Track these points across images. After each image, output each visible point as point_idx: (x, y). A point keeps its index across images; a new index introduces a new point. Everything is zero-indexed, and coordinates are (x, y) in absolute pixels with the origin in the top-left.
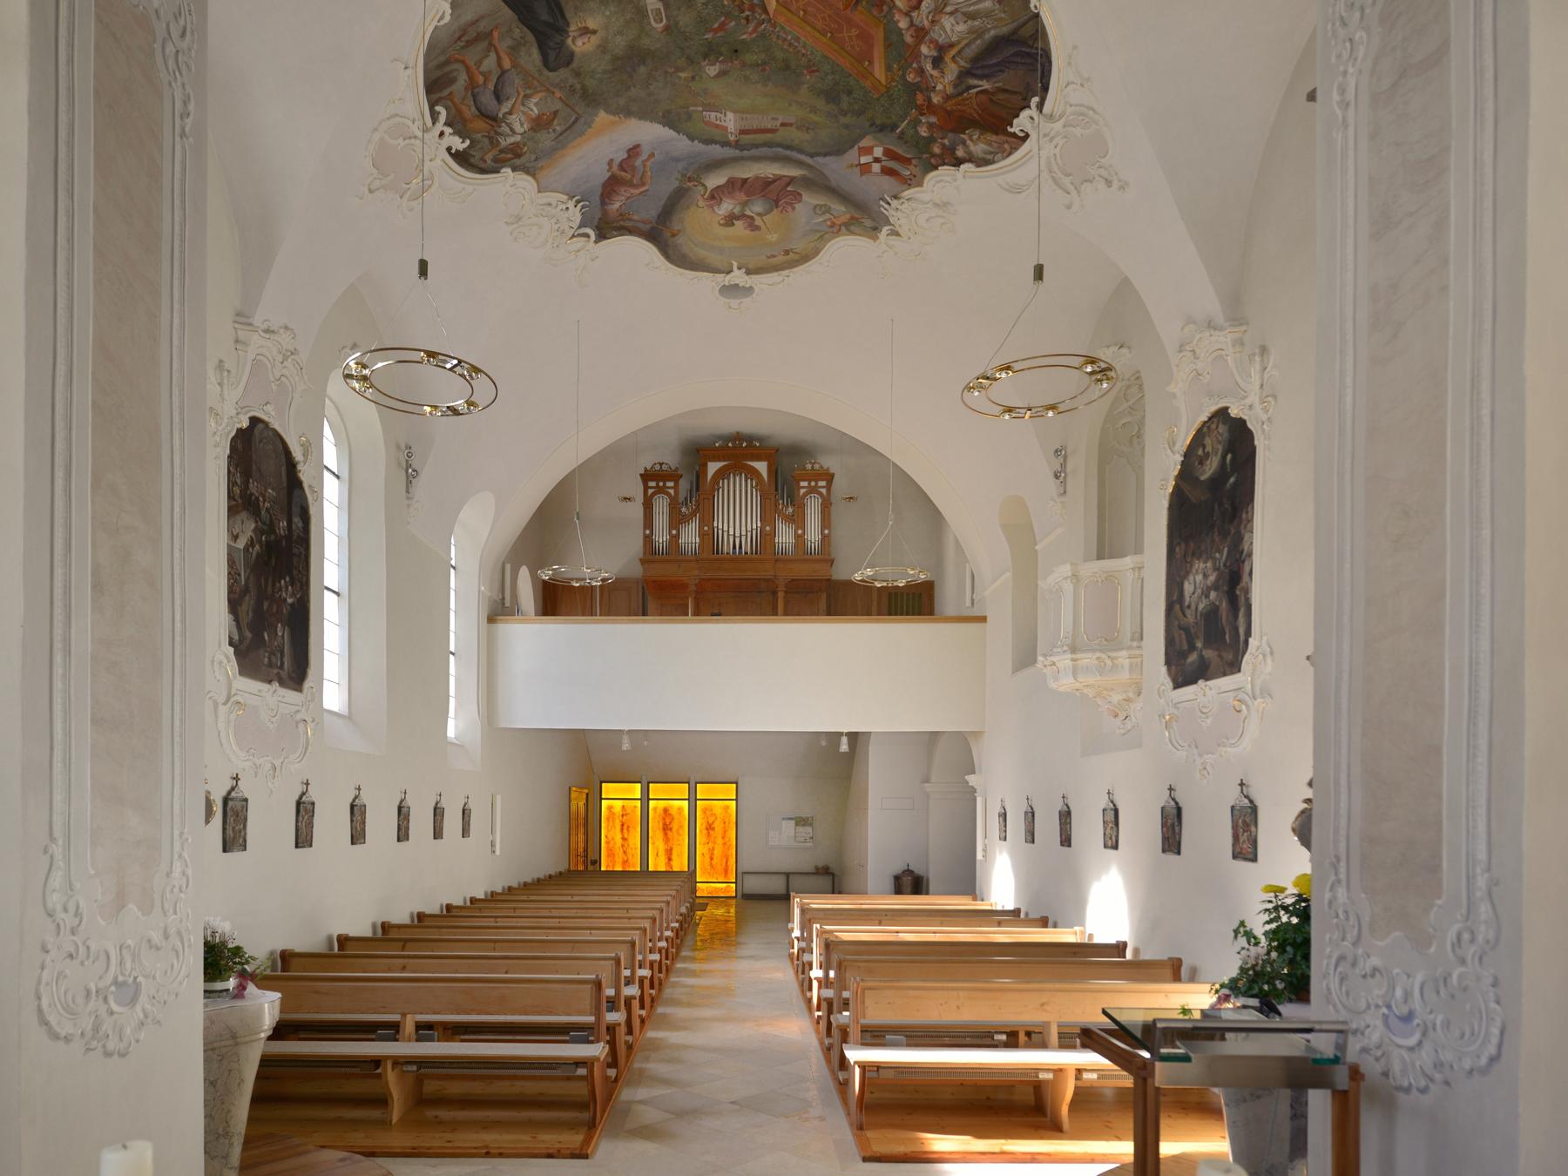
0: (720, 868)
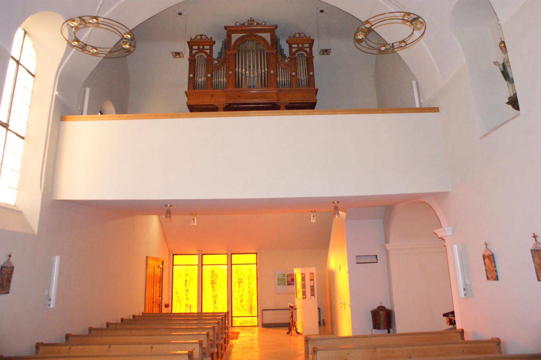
0: (247, 308)
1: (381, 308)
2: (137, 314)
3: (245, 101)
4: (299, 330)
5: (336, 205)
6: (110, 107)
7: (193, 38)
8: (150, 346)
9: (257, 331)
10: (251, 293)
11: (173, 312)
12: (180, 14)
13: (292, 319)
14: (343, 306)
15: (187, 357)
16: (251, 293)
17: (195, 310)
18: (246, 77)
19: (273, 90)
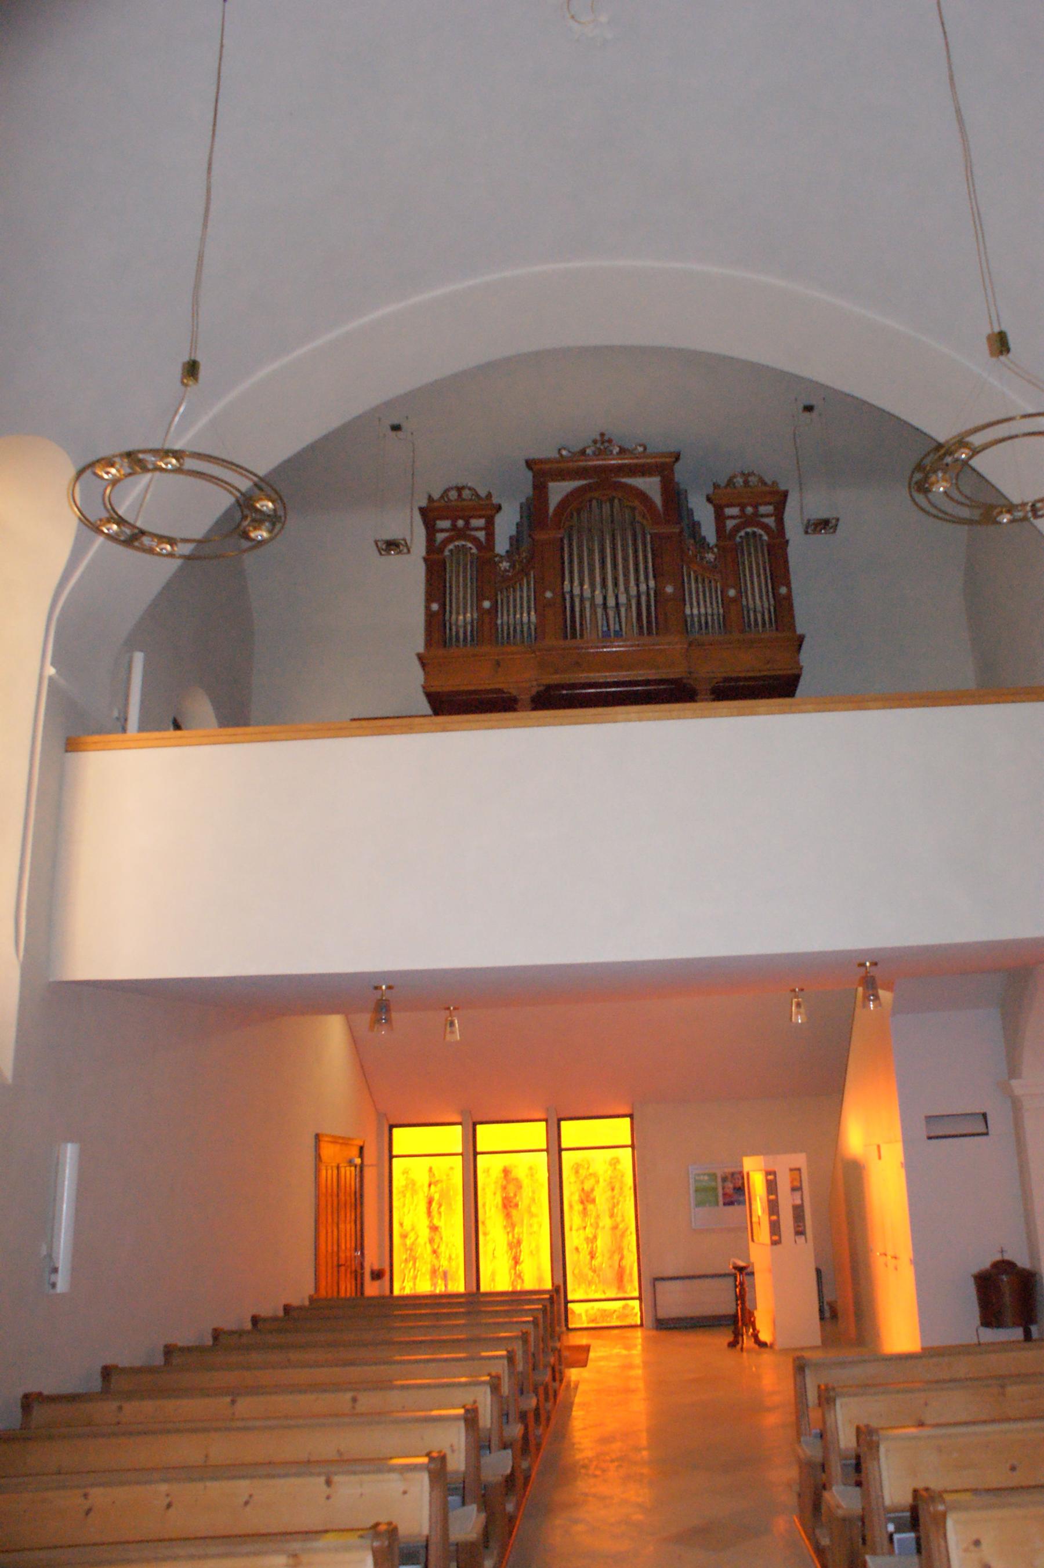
0: (610, 1274)
1: (1004, 1266)
2: (295, 1302)
3: (583, 677)
4: (765, 1336)
5: (869, 973)
6: (201, 707)
7: (436, 496)
8: (349, 1395)
9: (639, 1341)
10: (618, 1233)
11: (396, 1292)
12: (396, 428)
13: (743, 1303)
14: (891, 1262)
15: (462, 1424)
16: (618, 1233)
17: (459, 1286)
18: (593, 605)
19: (672, 644)
